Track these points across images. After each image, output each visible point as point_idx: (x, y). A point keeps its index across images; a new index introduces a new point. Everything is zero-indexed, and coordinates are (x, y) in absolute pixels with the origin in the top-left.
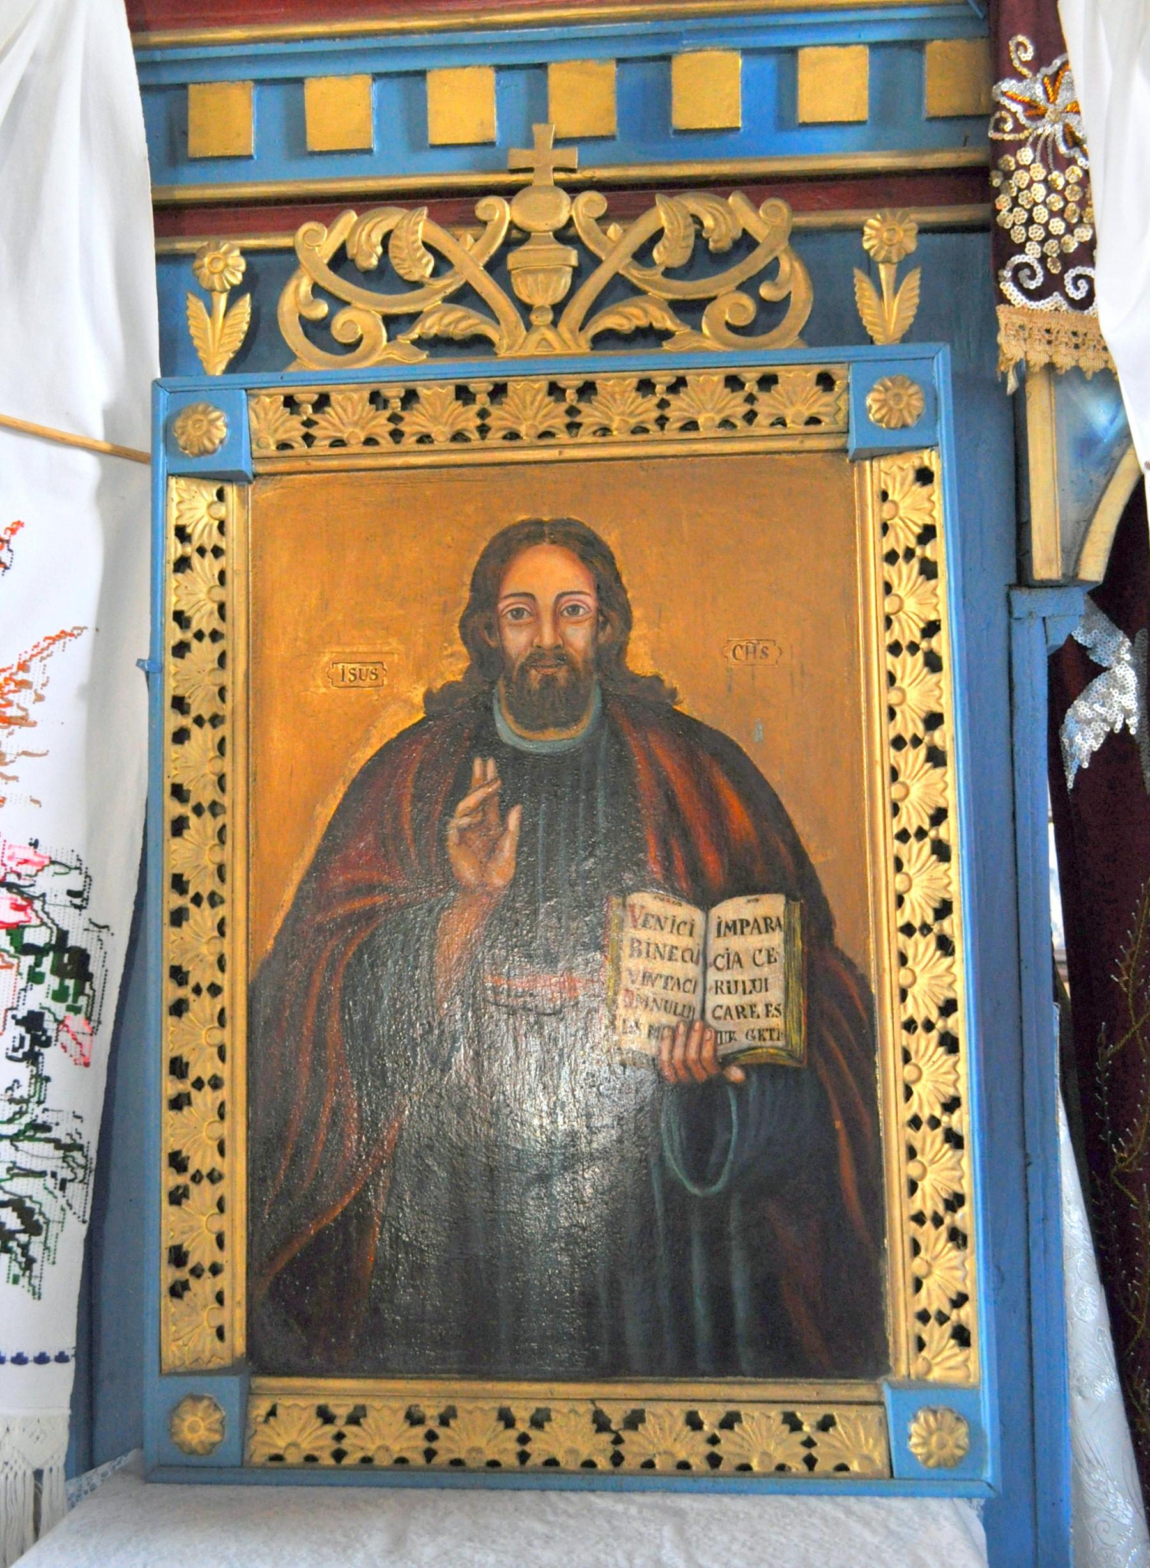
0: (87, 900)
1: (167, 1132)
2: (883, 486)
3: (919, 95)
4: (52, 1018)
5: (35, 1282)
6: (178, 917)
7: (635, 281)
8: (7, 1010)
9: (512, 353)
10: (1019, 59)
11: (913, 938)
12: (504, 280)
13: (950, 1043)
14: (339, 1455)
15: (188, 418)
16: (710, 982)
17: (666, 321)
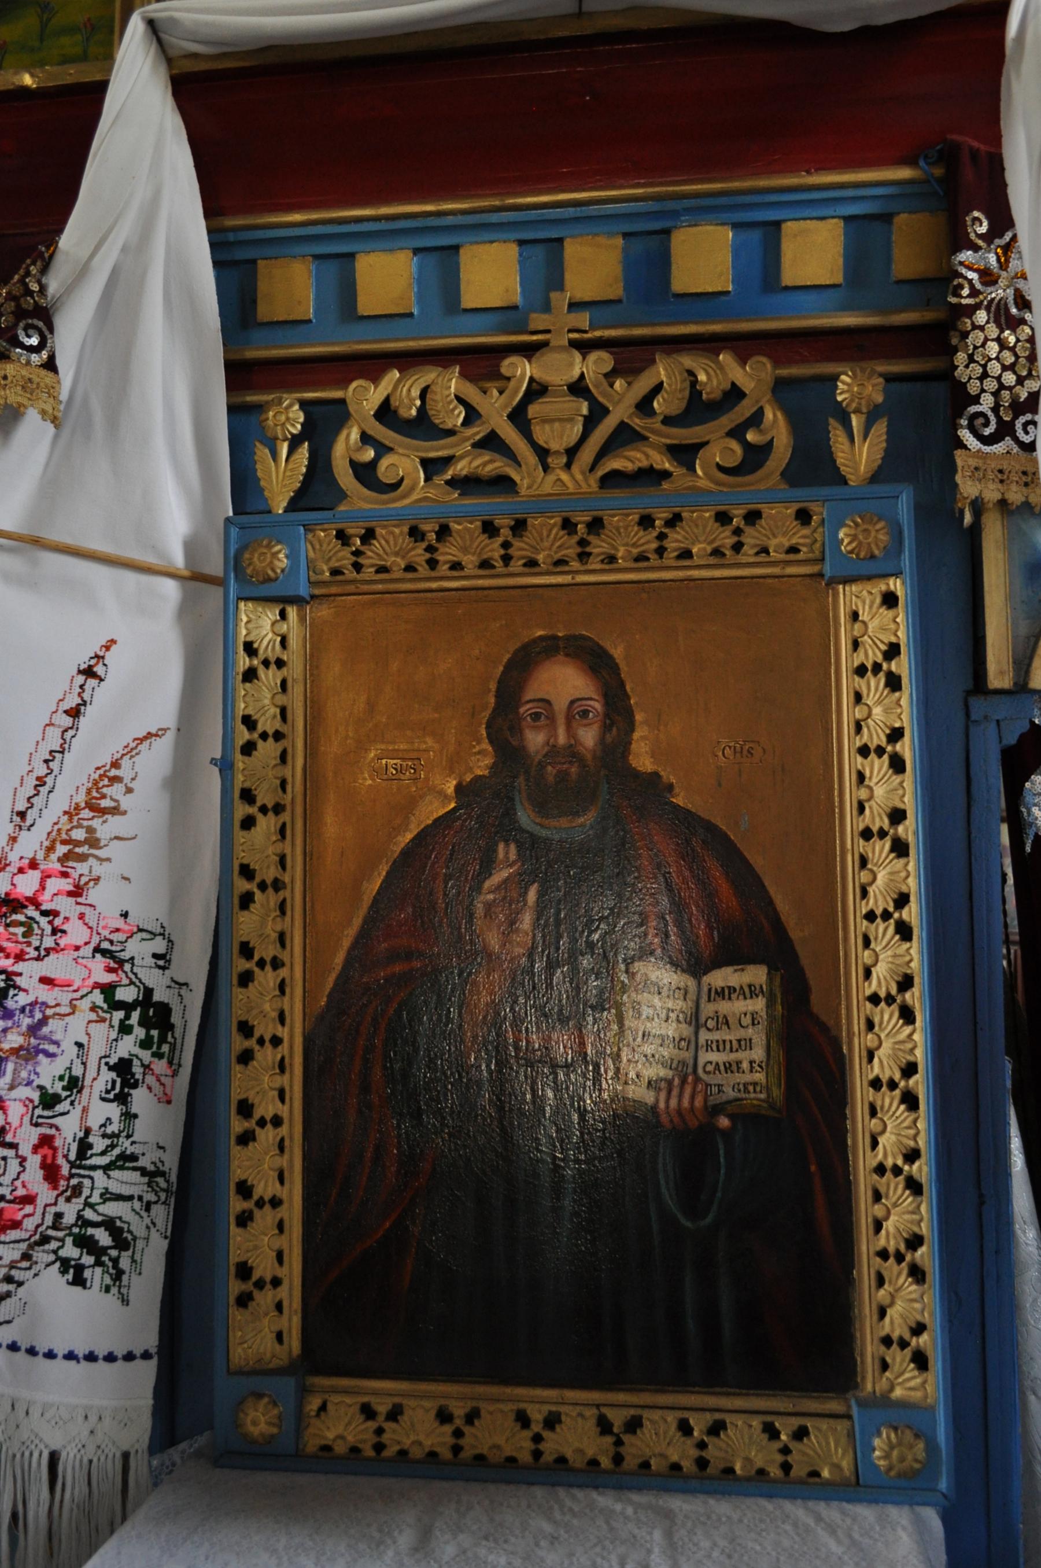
0: (169, 961)
1: (234, 1164)
2: (854, 608)
4: (139, 1063)
5: (124, 1291)
6: (245, 979)
7: (637, 428)
8: (101, 1058)
9: (532, 492)
10: (975, 232)
13: (910, 1100)
15: (255, 550)
16: (702, 1040)
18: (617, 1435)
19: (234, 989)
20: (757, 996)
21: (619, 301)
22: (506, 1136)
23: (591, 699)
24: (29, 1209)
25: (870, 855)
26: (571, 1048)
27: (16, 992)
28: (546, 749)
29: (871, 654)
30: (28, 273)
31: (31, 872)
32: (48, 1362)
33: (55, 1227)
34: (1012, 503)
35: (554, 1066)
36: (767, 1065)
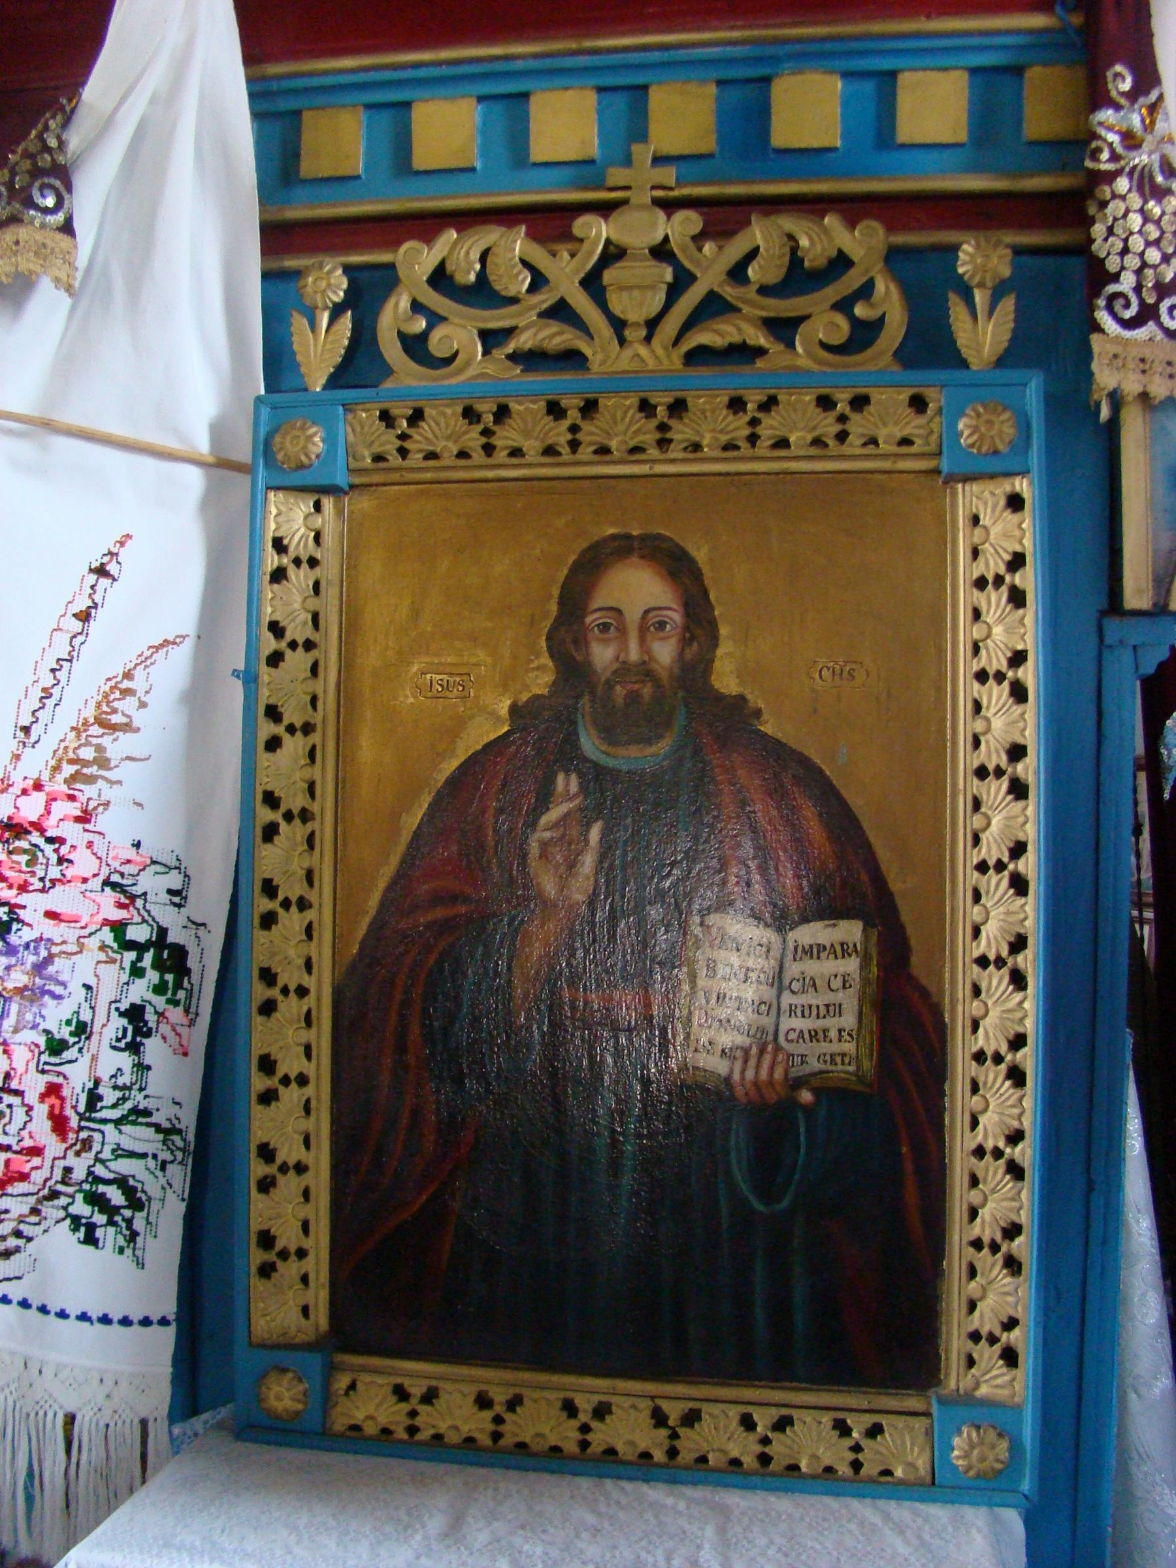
0: (186, 898)
1: (255, 1124)
2: (974, 510)
3: (1019, 122)
4: (152, 1010)
5: (139, 1253)
6: (268, 921)
7: (729, 299)
8: (111, 1003)
9: (604, 369)
10: (1117, 89)
11: (987, 971)
13: (1017, 1076)
14: (412, 1430)
15: (287, 433)
16: (785, 1005)
17: (760, 339)
18: (673, 1428)
19: (255, 931)
20: (850, 955)
21: (710, 156)
22: (558, 1103)
23: (669, 609)
24: (36, 1161)
25: (985, 797)
26: (636, 1010)
27: (20, 926)
28: (615, 666)
29: (993, 564)
30: (46, 128)
31: (35, 794)
32: (60, 1321)
33: (64, 1182)
34: (1155, 397)
35: (616, 1029)
36: (858, 1035)
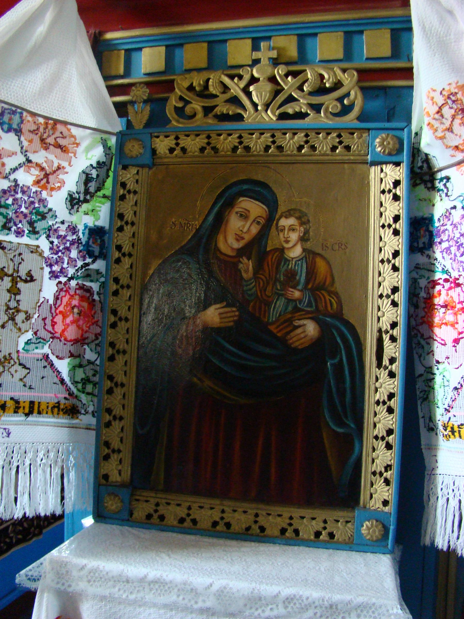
12: (249, 95)
